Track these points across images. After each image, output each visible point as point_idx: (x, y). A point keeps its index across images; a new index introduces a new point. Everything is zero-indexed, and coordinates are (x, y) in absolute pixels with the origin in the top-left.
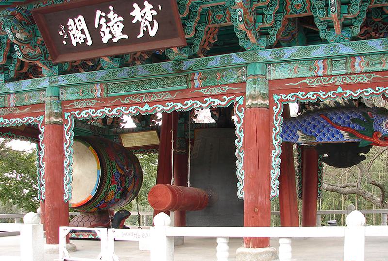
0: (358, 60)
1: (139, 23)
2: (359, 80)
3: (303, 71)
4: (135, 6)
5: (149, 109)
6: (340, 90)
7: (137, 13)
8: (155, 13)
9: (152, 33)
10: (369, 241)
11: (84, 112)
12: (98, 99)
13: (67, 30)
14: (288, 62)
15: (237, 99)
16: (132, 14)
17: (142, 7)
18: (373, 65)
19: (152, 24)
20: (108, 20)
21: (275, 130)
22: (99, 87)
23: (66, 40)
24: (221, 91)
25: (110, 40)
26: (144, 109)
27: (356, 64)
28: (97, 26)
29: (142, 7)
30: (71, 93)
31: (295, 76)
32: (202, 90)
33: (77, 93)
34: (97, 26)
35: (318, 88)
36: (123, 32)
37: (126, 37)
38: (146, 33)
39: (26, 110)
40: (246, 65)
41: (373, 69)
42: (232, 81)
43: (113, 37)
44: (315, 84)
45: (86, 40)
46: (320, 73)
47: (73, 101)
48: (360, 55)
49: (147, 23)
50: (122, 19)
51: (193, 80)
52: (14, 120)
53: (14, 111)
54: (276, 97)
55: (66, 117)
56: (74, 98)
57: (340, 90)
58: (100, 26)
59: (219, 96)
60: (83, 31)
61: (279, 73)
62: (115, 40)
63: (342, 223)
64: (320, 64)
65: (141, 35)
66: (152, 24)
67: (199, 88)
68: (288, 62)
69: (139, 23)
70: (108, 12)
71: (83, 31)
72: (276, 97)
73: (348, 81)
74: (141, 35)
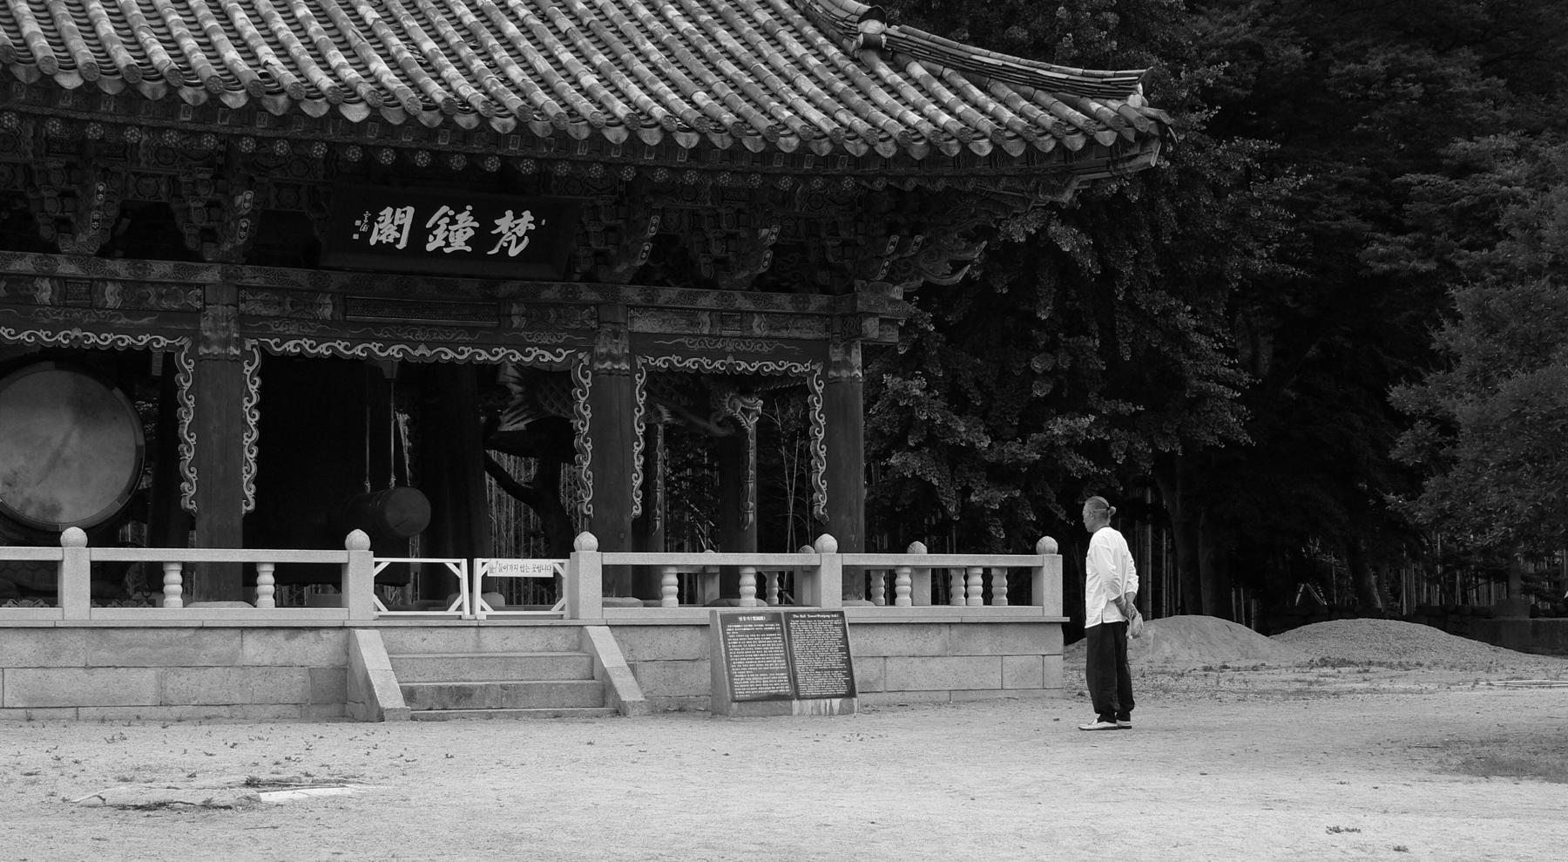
0: (757, 320)
1: (501, 235)
2: (757, 348)
3: (680, 325)
4: (509, 213)
5: (428, 353)
6: (730, 360)
7: (504, 223)
8: (532, 227)
9: (513, 252)
10: (98, 569)
11: (292, 343)
12: (324, 321)
13: (373, 220)
14: (660, 309)
15: (581, 356)
16: (497, 222)
17: (517, 216)
18: (777, 329)
19: (519, 240)
20: (453, 221)
21: (346, 348)
22: (328, 300)
23: (361, 234)
24: (554, 340)
25: (440, 249)
26: (417, 353)
27: (754, 325)
28: (429, 225)
29: (517, 216)
30: (265, 303)
31: (669, 331)
32: (524, 334)
33: (279, 304)
34: (429, 225)
35: (700, 354)
36: (467, 243)
37: (469, 249)
38: (504, 250)
39: (145, 321)
40: (597, 305)
41: (777, 334)
42: (573, 326)
43: (448, 245)
44: (696, 347)
45: (397, 240)
46: (706, 331)
47: (267, 317)
48: (759, 313)
49: (514, 238)
50: (476, 225)
51: (509, 315)
52: (111, 337)
53: (112, 317)
54: (639, 361)
55: (248, 347)
56: (272, 312)
57: (730, 360)
58: (436, 226)
59: (551, 348)
60: (400, 228)
61: (645, 325)
62: (447, 250)
63: (609, 599)
64: (705, 317)
65: (496, 251)
66: (519, 240)
67: (517, 329)
68: (660, 309)
69: (501, 235)
70: (460, 210)
71: (400, 228)
72: (639, 361)
73: (742, 348)
74: (496, 251)
